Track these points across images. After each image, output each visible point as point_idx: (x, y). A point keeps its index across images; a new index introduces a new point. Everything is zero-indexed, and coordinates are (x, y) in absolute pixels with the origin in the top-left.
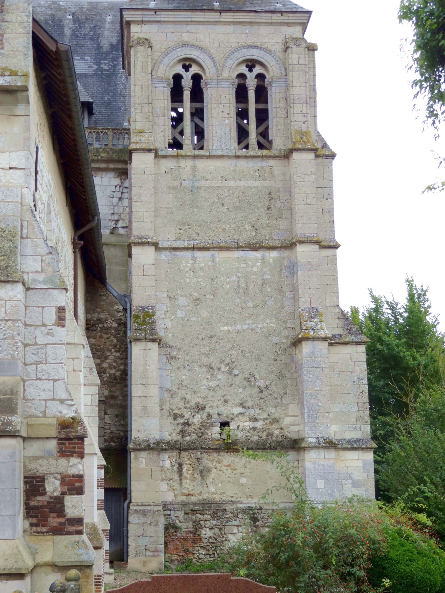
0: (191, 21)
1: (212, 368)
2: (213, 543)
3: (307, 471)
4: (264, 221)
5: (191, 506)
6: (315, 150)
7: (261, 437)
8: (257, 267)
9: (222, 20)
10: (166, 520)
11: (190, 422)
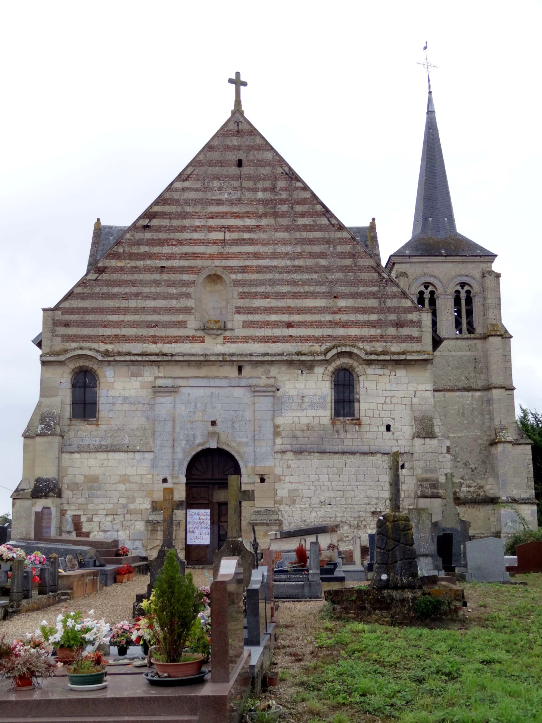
4: (472, 374)
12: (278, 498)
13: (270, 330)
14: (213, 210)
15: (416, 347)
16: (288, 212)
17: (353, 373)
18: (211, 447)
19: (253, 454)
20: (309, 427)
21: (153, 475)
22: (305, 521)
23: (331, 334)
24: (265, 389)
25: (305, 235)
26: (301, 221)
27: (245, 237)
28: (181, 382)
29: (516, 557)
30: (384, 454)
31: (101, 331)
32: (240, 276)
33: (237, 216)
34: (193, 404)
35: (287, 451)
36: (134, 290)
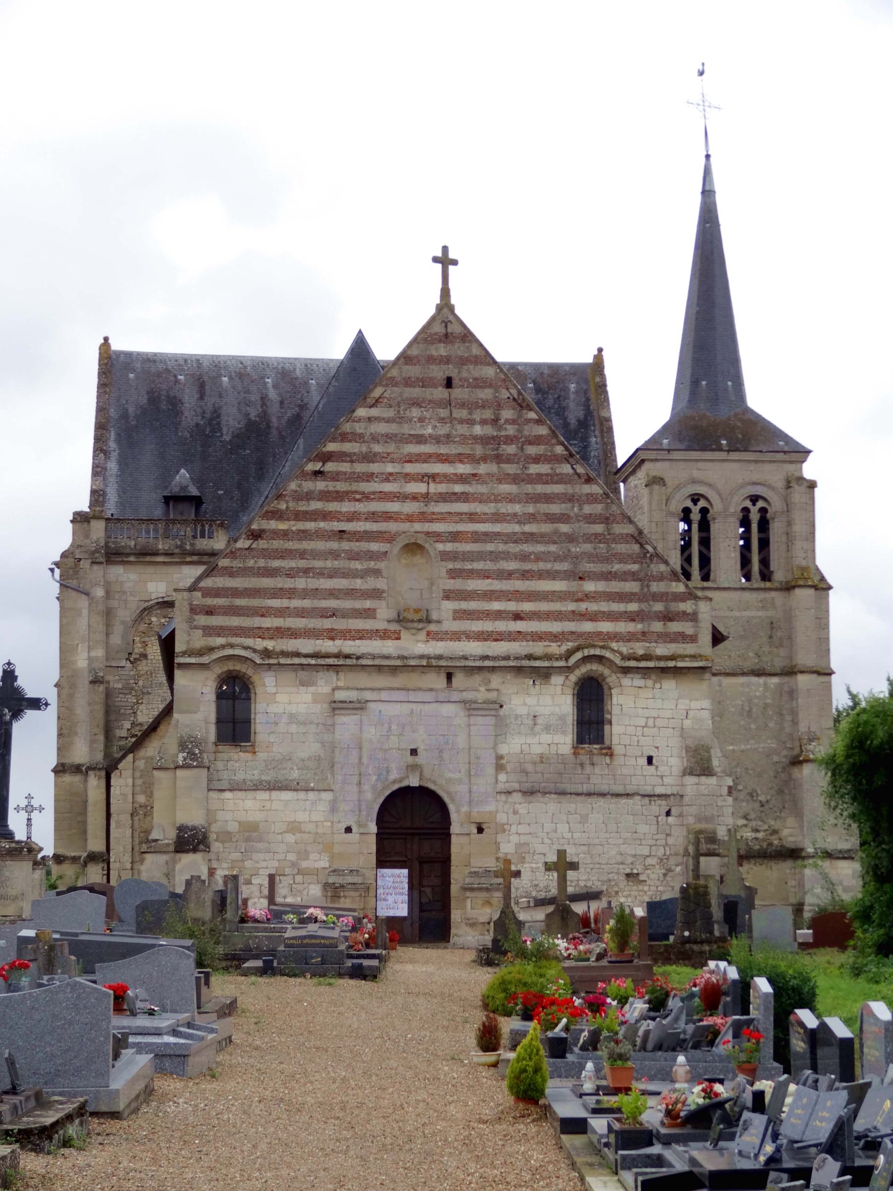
4: (766, 649)
6: (815, 587)
12: (500, 855)
13: (491, 623)
14: (412, 451)
15: (689, 649)
16: (515, 455)
17: (603, 683)
18: (411, 785)
19: (468, 795)
20: (542, 759)
21: (332, 823)
22: (536, 885)
23: (573, 630)
24: (484, 706)
25: (540, 488)
26: (534, 469)
27: (456, 491)
28: (368, 695)
29: (811, 931)
30: (644, 796)
31: (257, 622)
32: (449, 547)
33: (446, 460)
34: (386, 726)
35: (514, 791)
36: (302, 564)
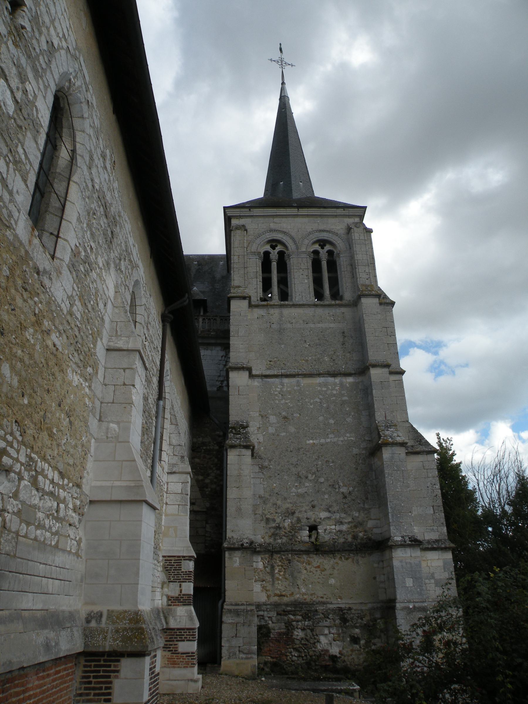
0: (277, 215)
1: (300, 477)
2: (306, 644)
3: (395, 570)
5: (284, 607)
7: (347, 539)
8: (337, 390)
9: (299, 214)
10: (260, 621)
11: (281, 526)
